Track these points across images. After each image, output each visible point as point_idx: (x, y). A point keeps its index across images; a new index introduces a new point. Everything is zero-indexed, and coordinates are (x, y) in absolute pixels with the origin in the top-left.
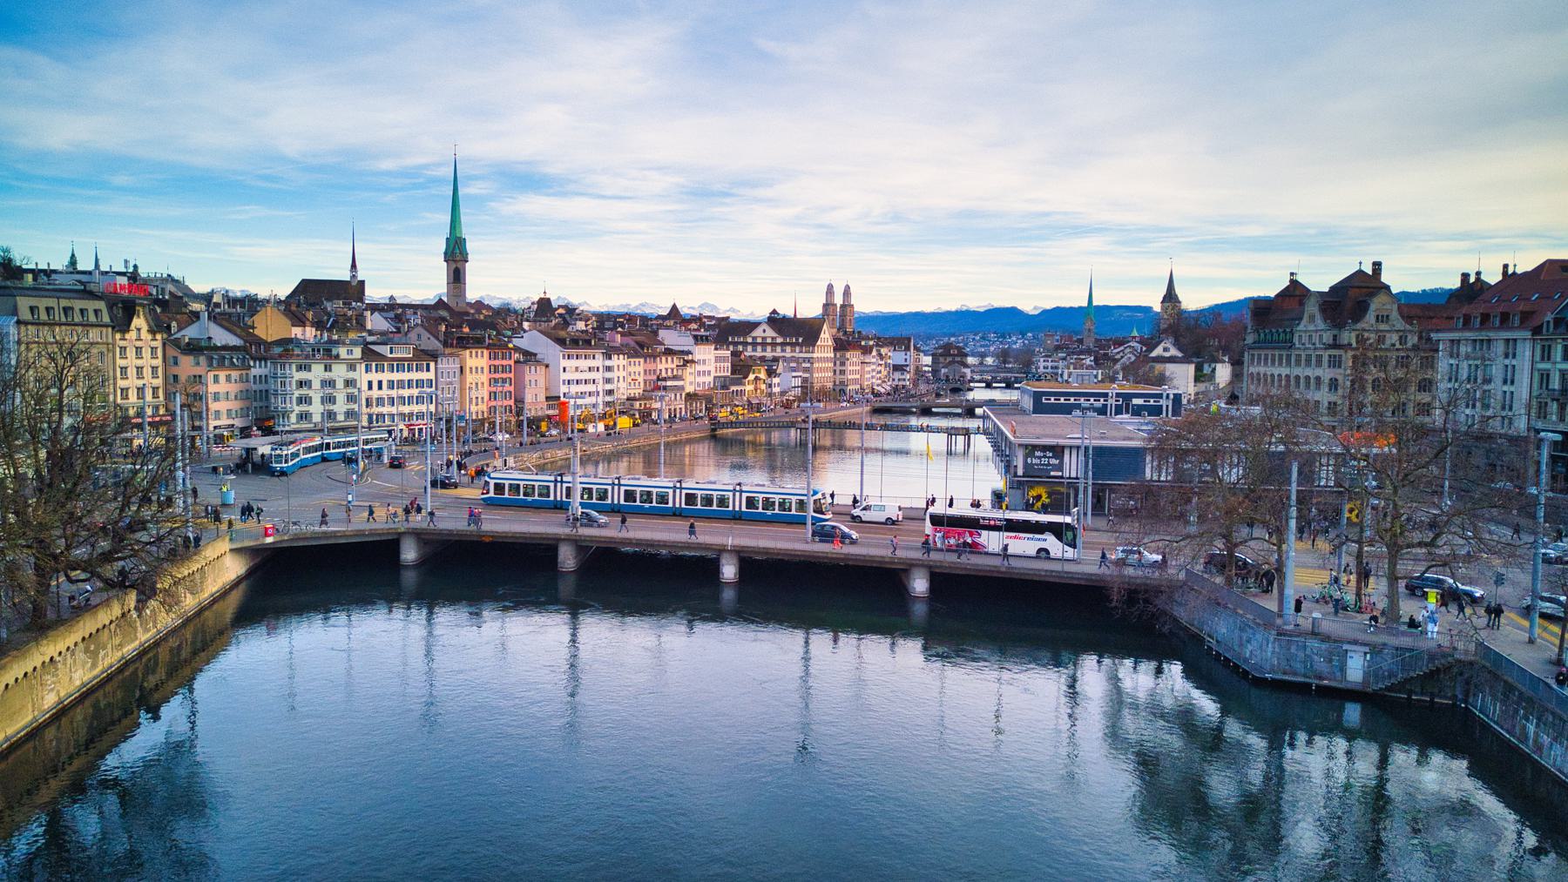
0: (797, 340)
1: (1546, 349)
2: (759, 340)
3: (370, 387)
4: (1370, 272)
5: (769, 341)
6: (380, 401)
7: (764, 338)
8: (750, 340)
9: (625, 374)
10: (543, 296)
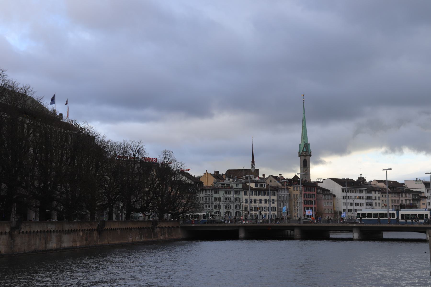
1: (428, 190)
4: (300, 175)
9: (380, 201)
10: (360, 177)
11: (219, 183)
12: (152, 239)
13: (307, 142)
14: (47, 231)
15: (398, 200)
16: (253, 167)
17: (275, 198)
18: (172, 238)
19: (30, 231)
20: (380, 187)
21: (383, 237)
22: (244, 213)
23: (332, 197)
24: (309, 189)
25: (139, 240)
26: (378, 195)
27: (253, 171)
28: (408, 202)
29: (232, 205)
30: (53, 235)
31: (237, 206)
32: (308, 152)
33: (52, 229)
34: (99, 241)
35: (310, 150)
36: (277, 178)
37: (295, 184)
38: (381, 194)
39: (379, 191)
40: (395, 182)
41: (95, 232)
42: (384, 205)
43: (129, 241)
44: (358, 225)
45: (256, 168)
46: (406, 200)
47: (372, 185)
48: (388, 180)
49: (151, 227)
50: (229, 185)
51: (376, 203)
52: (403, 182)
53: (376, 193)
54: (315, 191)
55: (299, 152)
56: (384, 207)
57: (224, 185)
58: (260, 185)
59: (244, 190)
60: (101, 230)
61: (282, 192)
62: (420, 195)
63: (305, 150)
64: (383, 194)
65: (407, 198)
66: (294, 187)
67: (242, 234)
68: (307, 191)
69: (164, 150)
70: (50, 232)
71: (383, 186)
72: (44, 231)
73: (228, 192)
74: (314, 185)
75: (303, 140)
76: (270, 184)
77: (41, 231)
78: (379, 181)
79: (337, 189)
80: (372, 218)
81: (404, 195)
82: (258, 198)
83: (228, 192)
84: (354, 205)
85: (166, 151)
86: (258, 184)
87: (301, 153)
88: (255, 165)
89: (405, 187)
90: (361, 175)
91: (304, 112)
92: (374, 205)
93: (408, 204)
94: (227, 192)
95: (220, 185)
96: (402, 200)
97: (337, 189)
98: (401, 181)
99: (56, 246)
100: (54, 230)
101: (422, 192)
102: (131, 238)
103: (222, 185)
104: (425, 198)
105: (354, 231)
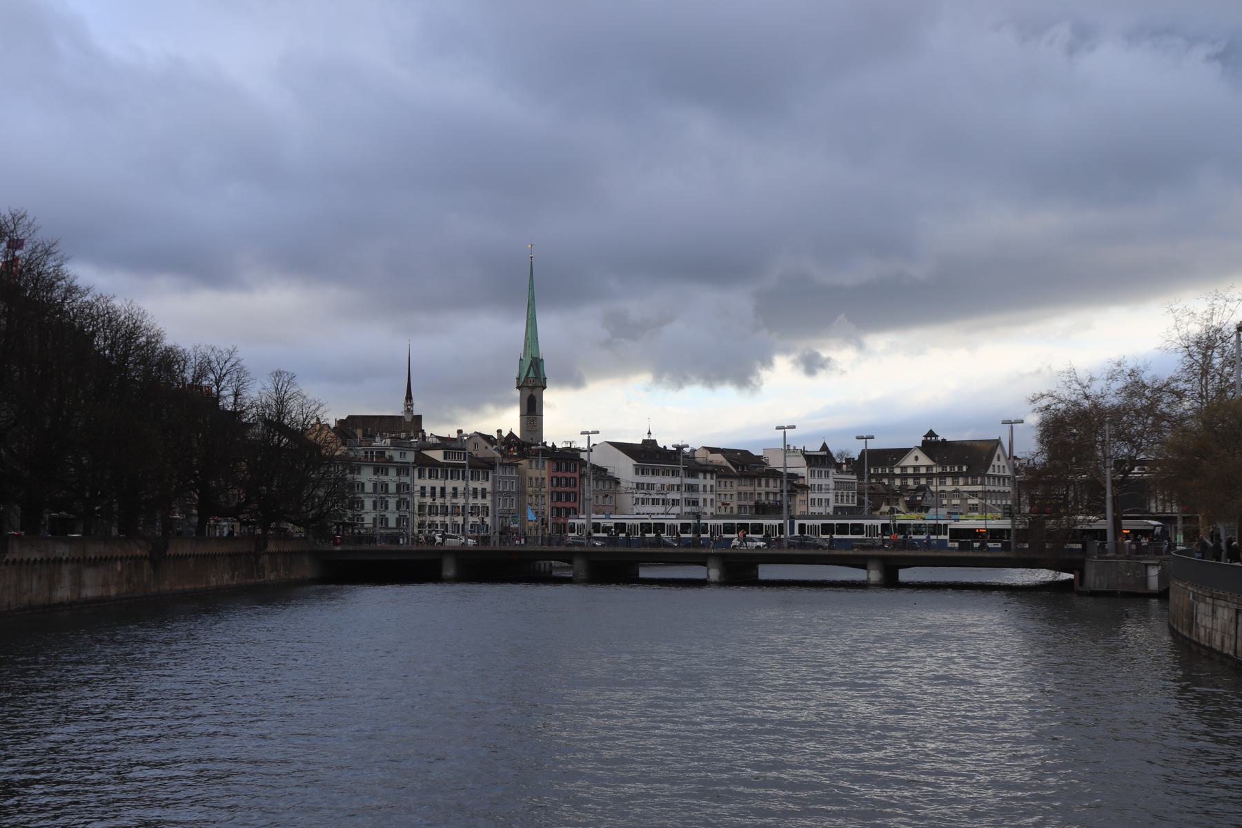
0: (960, 468)
2: (910, 471)
3: (423, 495)
5: (923, 471)
6: (433, 510)
7: (916, 468)
8: (897, 471)
9: (713, 496)
10: (646, 438)
11: (360, 448)
12: (254, 581)
13: (537, 356)
14: (55, 559)
15: (751, 494)
16: (409, 411)
17: (488, 486)
18: (293, 577)
19: (22, 560)
20: (715, 464)
21: (758, 576)
22: (417, 520)
23: (613, 484)
24: (564, 465)
25: (229, 583)
26: (709, 481)
27: (409, 419)
28: (771, 497)
29: (390, 500)
30: (66, 570)
31: (402, 503)
32: (540, 379)
33: (63, 554)
34: (152, 583)
35: (544, 375)
36: (492, 439)
37: (533, 454)
38: (717, 478)
39: (712, 472)
40: (746, 453)
41: (146, 563)
42: (723, 504)
43: (211, 585)
44: (584, 549)
45: (415, 414)
46: (767, 493)
47: (697, 459)
48: (868, 448)
49: (253, 551)
50: (384, 453)
51: (705, 500)
52: (760, 454)
53: (705, 478)
54: (575, 471)
55: (518, 379)
56: (723, 507)
57: (372, 453)
58: (455, 456)
59: (418, 466)
60: (158, 558)
61: (509, 472)
62: (795, 482)
63: (531, 375)
64: (720, 480)
65: (766, 490)
66: (531, 462)
67: (449, 571)
68: (558, 471)
69: (275, 369)
70: (58, 561)
71: (721, 462)
72: (49, 559)
73: (380, 471)
74: (567, 458)
75: (527, 351)
76: (474, 453)
77: (42, 559)
78: (713, 450)
79: (624, 468)
80: (850, 536)
81: (763, 482)
82: (450, 485)
83: (382, 472)
84: (682, 504)
85: (278, 374)
86: (449, 452)
87: (523, 380)
88: (412, 405)
89: (766, 464)
90: (649, 433)
91: (533, 285)
92: (701, 503)
93: (771, 502)
94: (378, 471)
95: (362, 453)
96: (759, 494)
97: (624, 468)
98: (757, 453)
99: (69, 595)
100: (67, 559)
101: (799, 475)
102: (214, 577)
103: (366, 453)
104: (805, 488)
105: (709, 565)
